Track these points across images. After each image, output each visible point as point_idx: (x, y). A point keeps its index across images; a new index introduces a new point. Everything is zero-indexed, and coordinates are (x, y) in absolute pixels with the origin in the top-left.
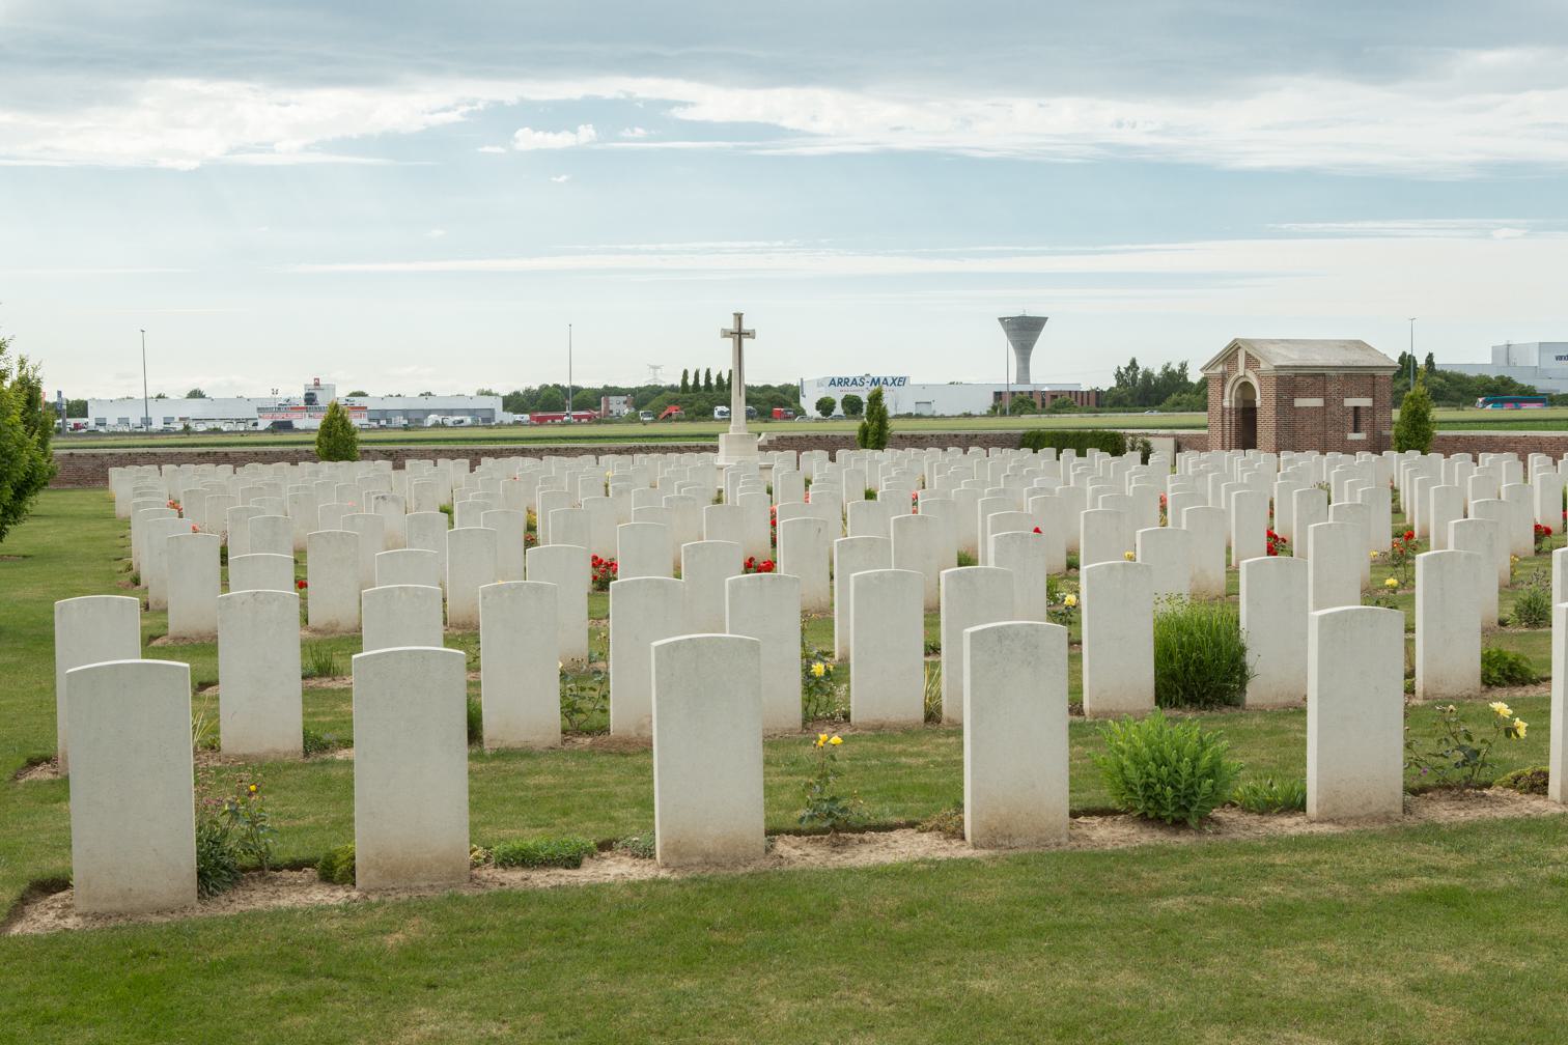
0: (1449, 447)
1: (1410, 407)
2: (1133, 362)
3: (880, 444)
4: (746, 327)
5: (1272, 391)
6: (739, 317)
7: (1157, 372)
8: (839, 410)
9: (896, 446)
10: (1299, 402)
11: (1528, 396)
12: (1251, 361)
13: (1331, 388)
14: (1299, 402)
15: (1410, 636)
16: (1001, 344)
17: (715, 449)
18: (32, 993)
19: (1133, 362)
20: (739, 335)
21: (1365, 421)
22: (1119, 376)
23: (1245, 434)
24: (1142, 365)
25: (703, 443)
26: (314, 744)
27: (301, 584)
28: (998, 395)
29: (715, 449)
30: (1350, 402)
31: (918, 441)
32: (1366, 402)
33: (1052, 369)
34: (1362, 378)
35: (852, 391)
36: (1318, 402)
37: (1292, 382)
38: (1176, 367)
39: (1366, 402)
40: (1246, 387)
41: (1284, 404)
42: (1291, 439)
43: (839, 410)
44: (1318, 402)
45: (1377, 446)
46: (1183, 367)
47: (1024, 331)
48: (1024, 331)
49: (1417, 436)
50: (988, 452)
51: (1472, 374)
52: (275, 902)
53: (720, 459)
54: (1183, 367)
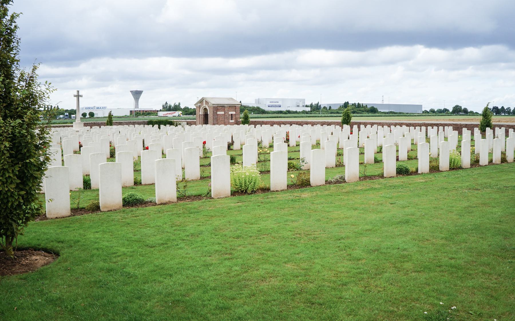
0: (255, 124)
1: (246, 115)
2: (166, 103)
3: (111, 125)
4: (80, 94)
6: (78, 91)
7: (173, 105)
8: (88, 116)
9: (115, 125)
10: (218, 113)
11: (264, 112)
12: (207, 103)
13: (226, 109)
14: (218, 113)
16: (131, 98)
17: (72, 126)
18: (456, 252)
19: (166, 103)
20: (78, 96)
21: (234, 117)
22: (163, 106)
23: (206, 121)
24: (169, 103)
27: (63, 161)
29: (72, 126)
30: (230, 113)
31: (120, 124)
32: (234, 113)
33: (144, 105)
34: (233, 107)
35: (91, 111)
36: (223, 113)
37: (217, 108)
39: (234, 113)
40: (205, 109)
42: (216, 122)
43: (88, 116)
44: (223, 113)
45: (237, 123)
47: (137, 94)
48: (137, 94)
49: (246, 121)
54: (179, 104)
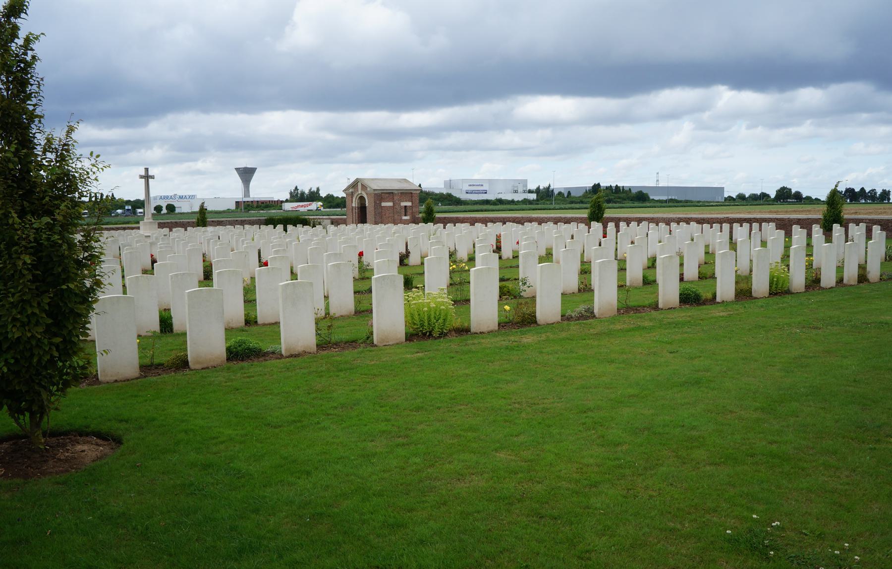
0: (445, 222)
1: (430, 207)
5: (372, 200)
6: (147, 170)
7: (307, 192)
8: (164, 211)
9: (211, 225)
10: (383, 204)
12: (364, 187)
13: (396, 198)
14: (383, 204)
15: (363, 286)
16: (236, 181)
17: (138, 228)
20: (147, 177)
21: (409, 211)
23: (362, 218)
25: (124, 226)
26: (358, 312)
28: (237, 203)
29: (138, 228)
30: (403, 204)
32: (409, 204)
34: (407, 194)
36: (390, 204)
38: (314, 189)
39: (409, 204)
40: (362, 198)
41: (377, 205)
42: (380, 220)
43: (164, 211)
44: (390, 204)
45: (415, 221)
46: (318, 189)
47: (246, 174)
48: (246, 174)
49: (429, 217)
50: (721, 228)
51: (437, 192)
52: (612, 326)
53: (141, 232)
54: (318, 189)
